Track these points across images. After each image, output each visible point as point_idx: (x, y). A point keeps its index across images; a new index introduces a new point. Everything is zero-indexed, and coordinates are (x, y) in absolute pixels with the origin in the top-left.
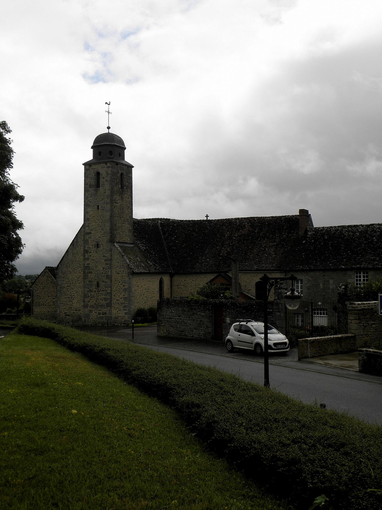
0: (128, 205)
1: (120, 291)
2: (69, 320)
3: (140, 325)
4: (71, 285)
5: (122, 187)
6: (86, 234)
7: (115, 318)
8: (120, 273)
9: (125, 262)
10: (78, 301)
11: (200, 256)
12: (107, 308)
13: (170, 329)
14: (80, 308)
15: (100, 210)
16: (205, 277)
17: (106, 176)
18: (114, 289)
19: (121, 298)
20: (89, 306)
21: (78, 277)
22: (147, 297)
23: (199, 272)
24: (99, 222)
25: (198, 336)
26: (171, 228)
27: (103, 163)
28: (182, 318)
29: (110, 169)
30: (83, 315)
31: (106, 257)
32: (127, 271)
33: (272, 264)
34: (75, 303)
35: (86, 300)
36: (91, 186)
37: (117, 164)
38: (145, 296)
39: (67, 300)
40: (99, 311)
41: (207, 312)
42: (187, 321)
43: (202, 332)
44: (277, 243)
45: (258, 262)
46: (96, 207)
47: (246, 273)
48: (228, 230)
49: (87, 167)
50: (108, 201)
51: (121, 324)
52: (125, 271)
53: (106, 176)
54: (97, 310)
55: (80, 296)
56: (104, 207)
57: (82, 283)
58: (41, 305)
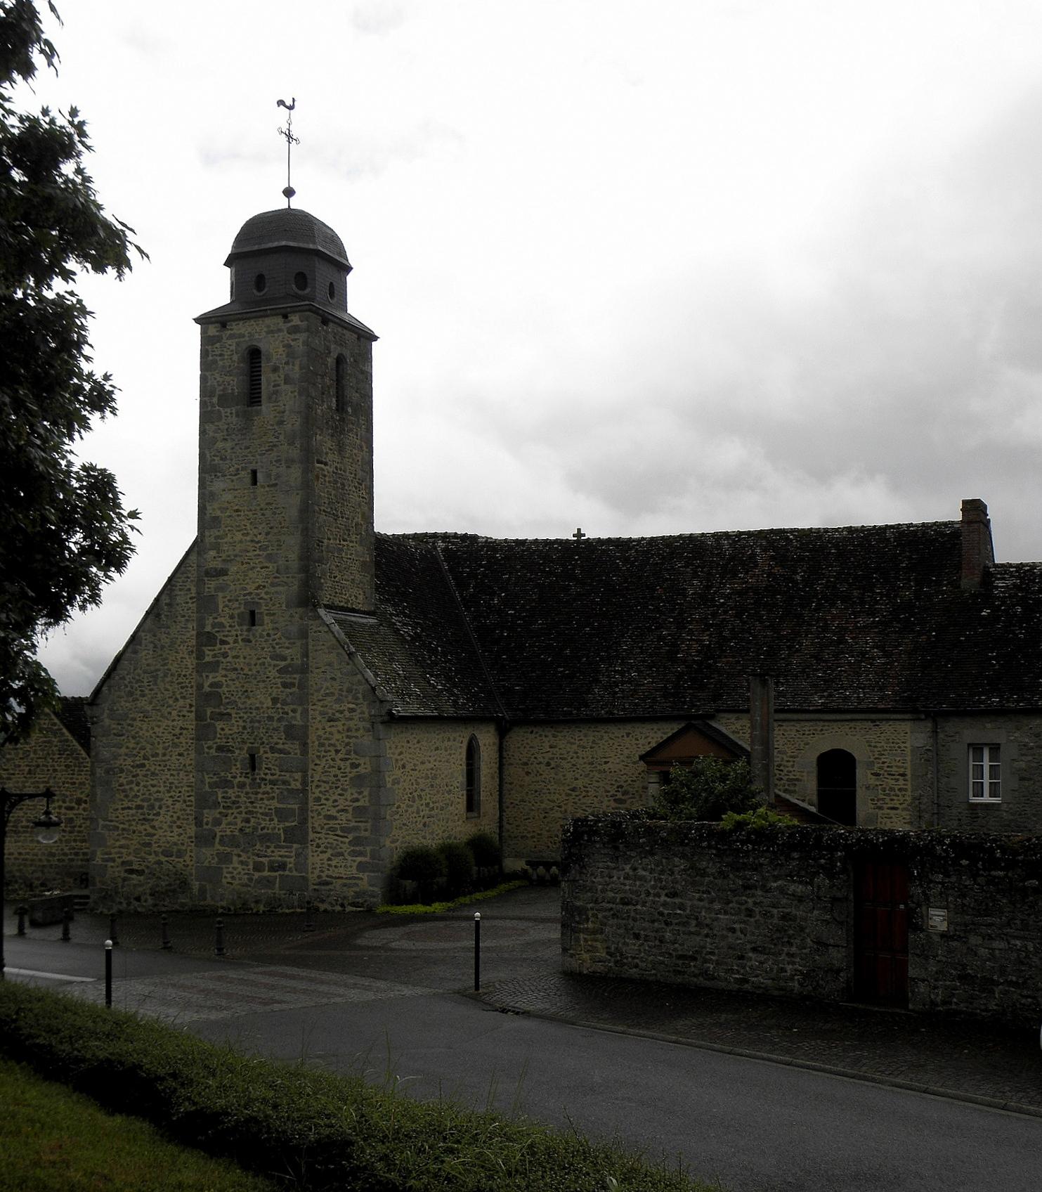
0: (360, 472)
1: (339, 784)
2: (141, 889)
3: (420, 909)
4: (146, 762)
5: (341, 408)
6: (207, 573)
7: (320, 884)
8: (337, 720)
9: (359, 677)
10: (175, 819)
11: (602, 660)
12: (287, 847)
13: (625, 944)
14: (183, 844)
15: (263, 487)
16: (628, 735)
17: (287, 363)
18: (317, 777)
19: (343, 810)
20: (217, 840)
21: (177, 731)
22: (431, 805)
23: (605, 716)
24: (255, 531)
25: (773, 979)
26: (482, 566)
27: (274, 313)
28: (689, 903)
29: (302, 337)
30: (194, 871)
31: (285, 659)
32: (366, 711)
33: (881, 689)
34: (165, 827)
35: (209, 815)
36: (224, 400)
37: (325, 322)
38: (423, 802)
39: (133, 815)
40: (258, 855)
41: (821, 879)
42: (713, 915)
43: (794, 963)
44: (884, 616)
45: (825, 681)
46: (246, 476)
47: (784, 721)
48: (695, 573)
49: (213, 330)
50: (295, 453)
51: (342, 905)
52: (359, 711)
53: (287, 363)
54: (250, 854)
55: (185, 801)
56: (278, 476)
57: (193, 756)
58: (24, 832)
